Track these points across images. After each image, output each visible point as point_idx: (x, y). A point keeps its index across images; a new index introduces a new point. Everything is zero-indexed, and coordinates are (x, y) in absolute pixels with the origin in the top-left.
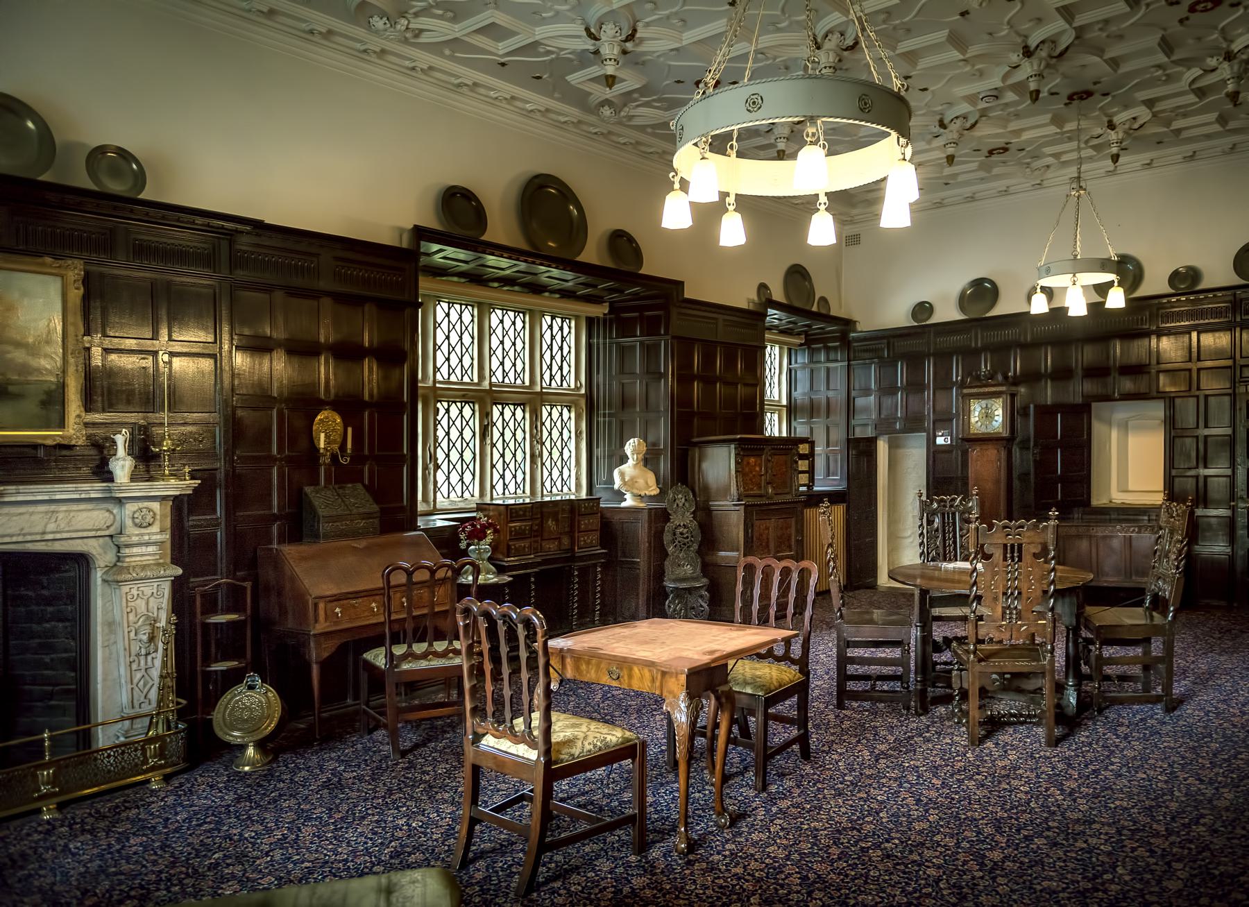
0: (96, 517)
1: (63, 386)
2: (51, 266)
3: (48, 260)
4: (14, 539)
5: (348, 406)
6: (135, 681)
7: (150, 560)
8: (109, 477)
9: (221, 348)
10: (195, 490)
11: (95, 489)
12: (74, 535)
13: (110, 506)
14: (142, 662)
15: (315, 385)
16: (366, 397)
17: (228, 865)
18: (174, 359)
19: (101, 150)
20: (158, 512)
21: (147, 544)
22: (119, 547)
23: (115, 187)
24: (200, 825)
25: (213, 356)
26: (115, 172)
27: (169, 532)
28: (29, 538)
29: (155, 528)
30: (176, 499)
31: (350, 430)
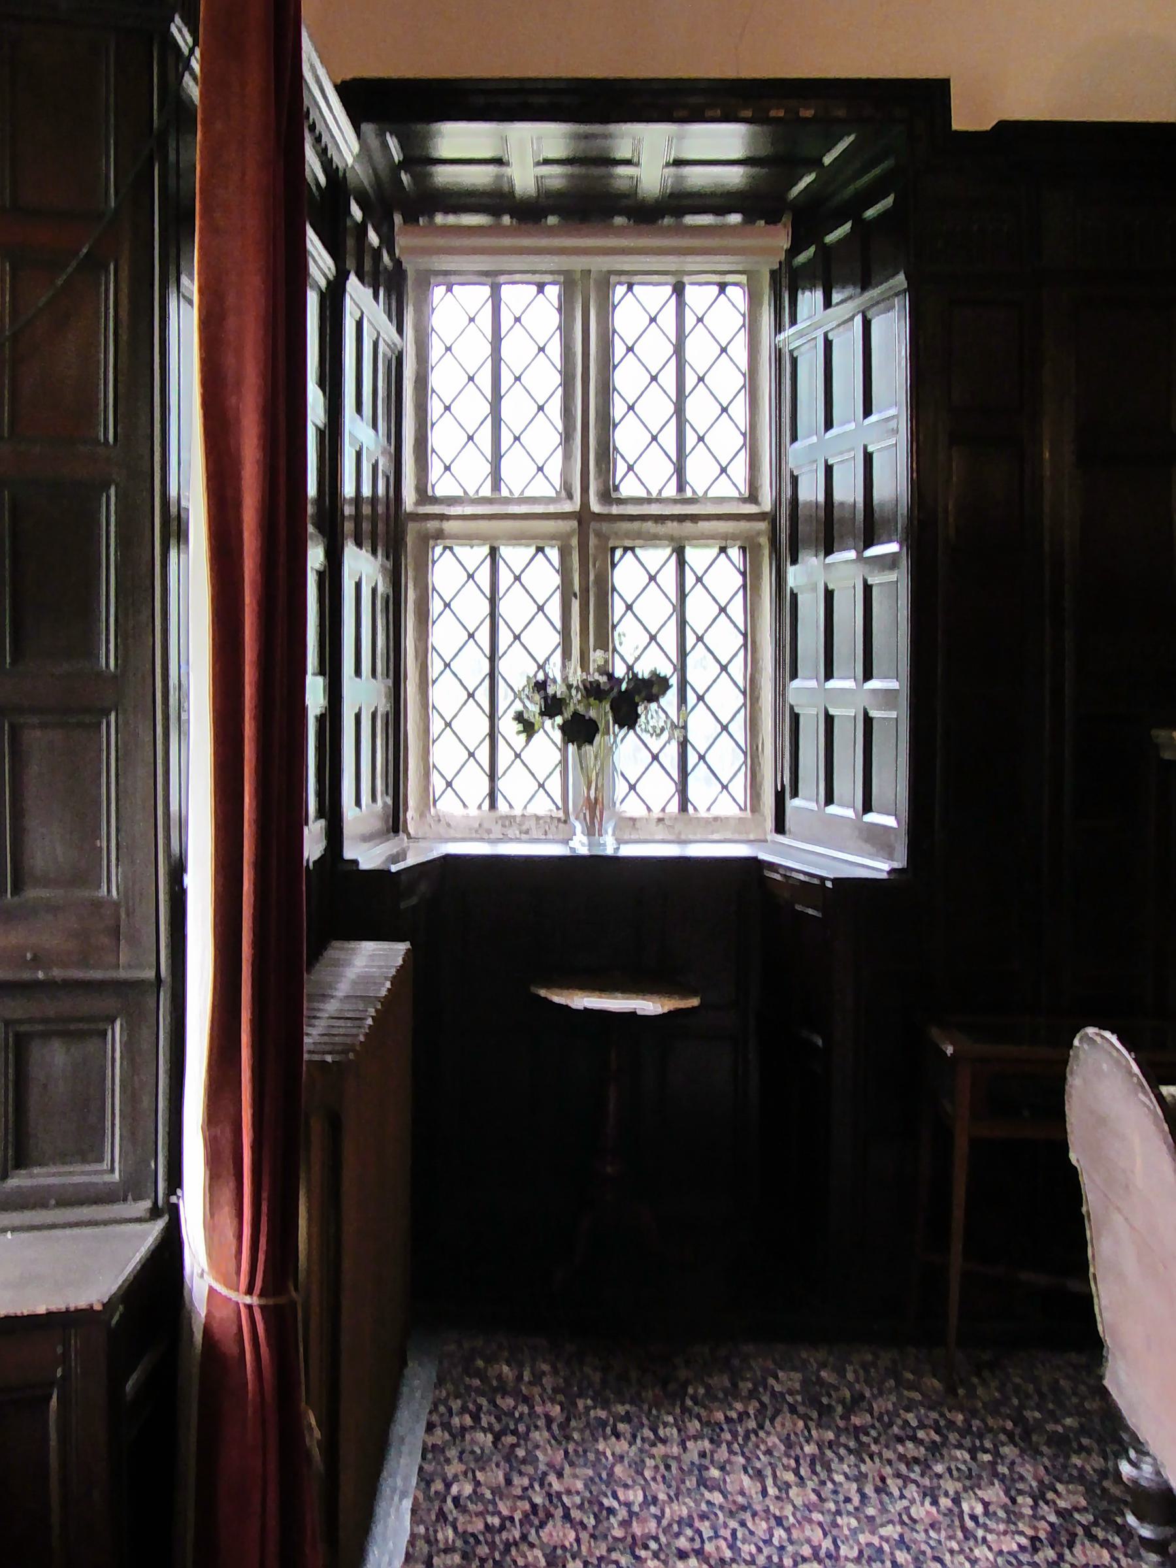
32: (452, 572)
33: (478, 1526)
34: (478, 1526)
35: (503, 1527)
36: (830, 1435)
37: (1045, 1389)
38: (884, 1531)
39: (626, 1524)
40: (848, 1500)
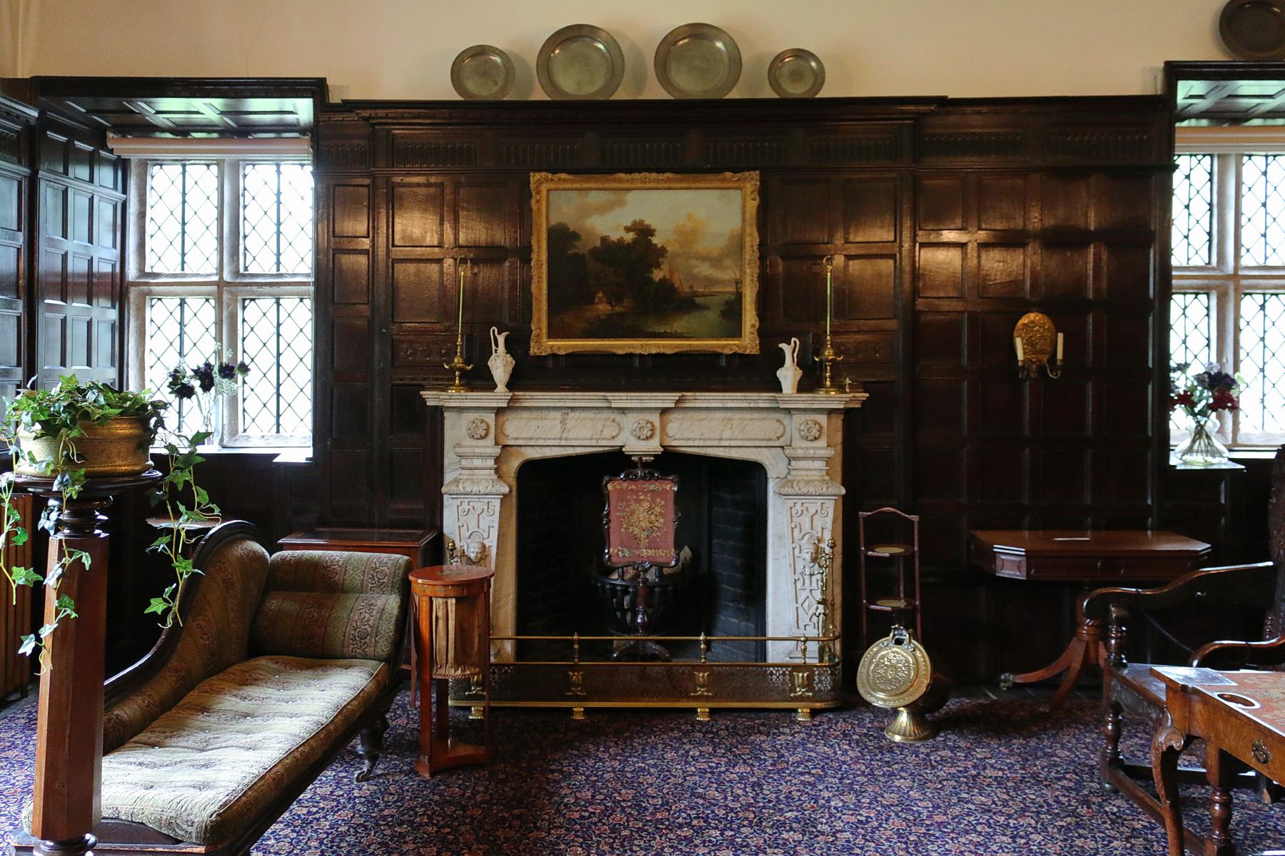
0: (764, 427)
1: (739, 296)
2: (730, 180)
3: (729, 174)
4: (696, 443)
5: (1062, 304)
6: (800, 601)
7: (815, 475)
8: (777, 387)
9: (901, 247)
10: (864, 403)
11: (762, 399)
12: (747, 443)
13: (781, 416)
14: (807, 582)
15: (1080, 282)
16: (1090, 295)
17: (791, 829)
18: (851, 263)
19: (780, 58)
20: (825, 425)
21: (813, 459)
22: (789, 459)
23: (795, 90)
24: (1059, 779)
25: (892, 256)
26: (796, 76)
27: (839, 448)
28: (708, 443)
29: (822, 443)
30: (847, 413)
31: (1060, 336)
32: (160, 314)
33: (577, 815)
34: (577, 815)
35: (590, 817)
36: (923, 830)
37: (1050, 801)
38: (788, 814)
39: (652, 814)
40: (770, 802)
